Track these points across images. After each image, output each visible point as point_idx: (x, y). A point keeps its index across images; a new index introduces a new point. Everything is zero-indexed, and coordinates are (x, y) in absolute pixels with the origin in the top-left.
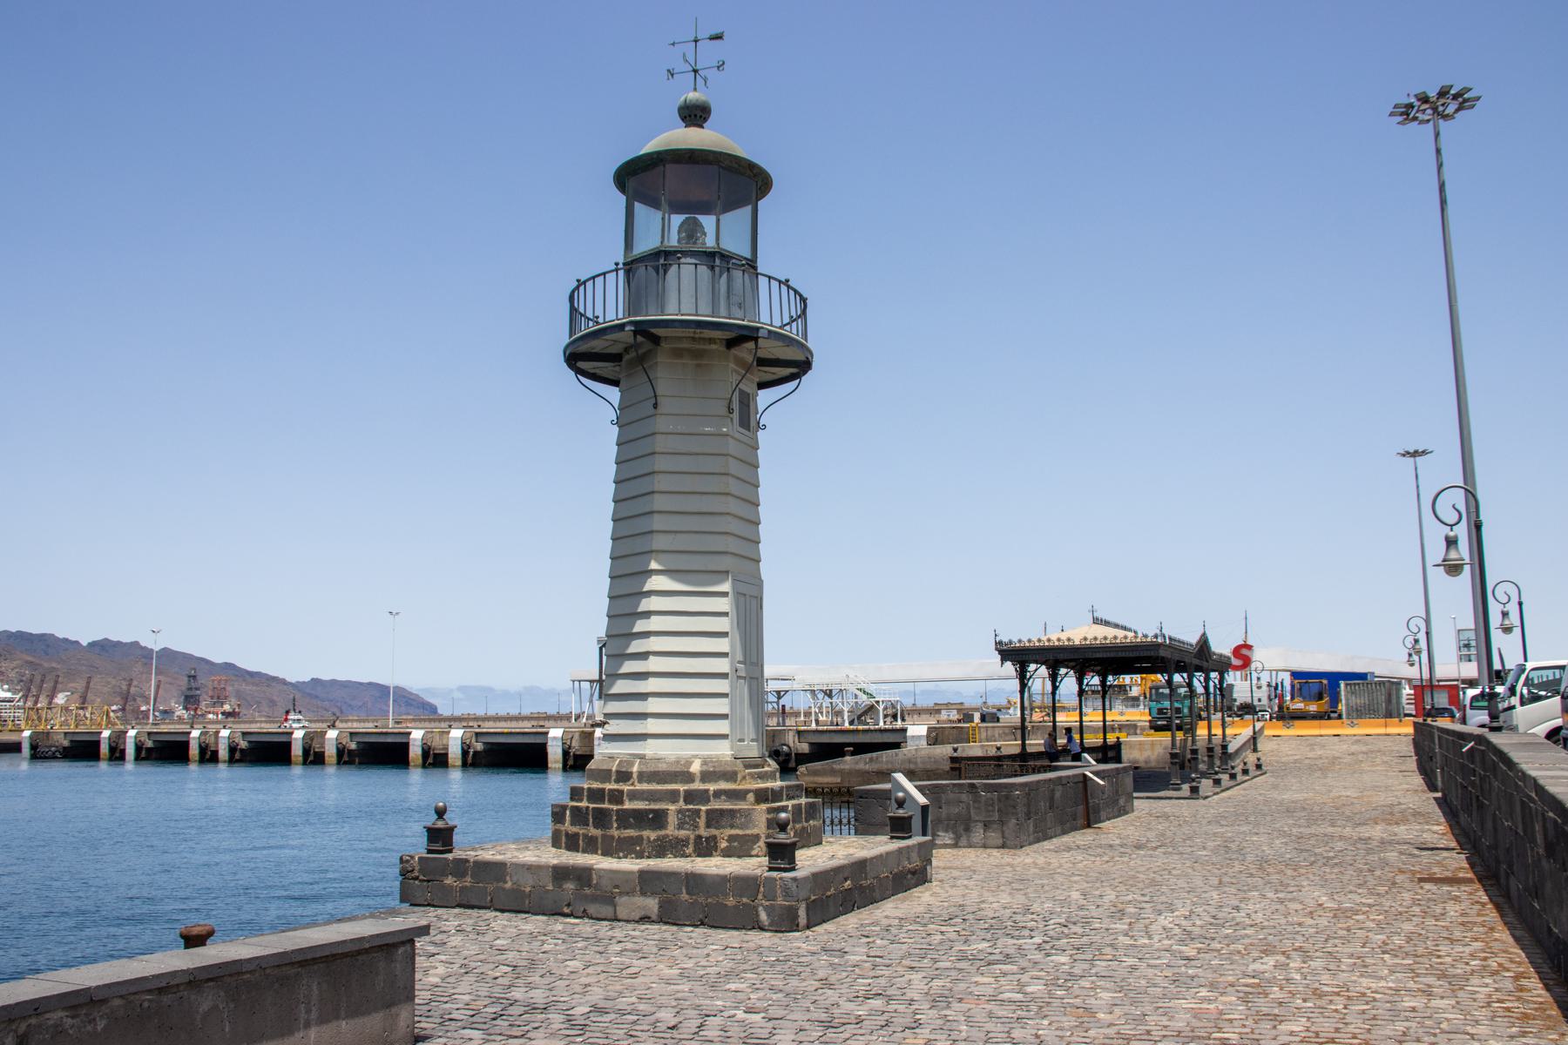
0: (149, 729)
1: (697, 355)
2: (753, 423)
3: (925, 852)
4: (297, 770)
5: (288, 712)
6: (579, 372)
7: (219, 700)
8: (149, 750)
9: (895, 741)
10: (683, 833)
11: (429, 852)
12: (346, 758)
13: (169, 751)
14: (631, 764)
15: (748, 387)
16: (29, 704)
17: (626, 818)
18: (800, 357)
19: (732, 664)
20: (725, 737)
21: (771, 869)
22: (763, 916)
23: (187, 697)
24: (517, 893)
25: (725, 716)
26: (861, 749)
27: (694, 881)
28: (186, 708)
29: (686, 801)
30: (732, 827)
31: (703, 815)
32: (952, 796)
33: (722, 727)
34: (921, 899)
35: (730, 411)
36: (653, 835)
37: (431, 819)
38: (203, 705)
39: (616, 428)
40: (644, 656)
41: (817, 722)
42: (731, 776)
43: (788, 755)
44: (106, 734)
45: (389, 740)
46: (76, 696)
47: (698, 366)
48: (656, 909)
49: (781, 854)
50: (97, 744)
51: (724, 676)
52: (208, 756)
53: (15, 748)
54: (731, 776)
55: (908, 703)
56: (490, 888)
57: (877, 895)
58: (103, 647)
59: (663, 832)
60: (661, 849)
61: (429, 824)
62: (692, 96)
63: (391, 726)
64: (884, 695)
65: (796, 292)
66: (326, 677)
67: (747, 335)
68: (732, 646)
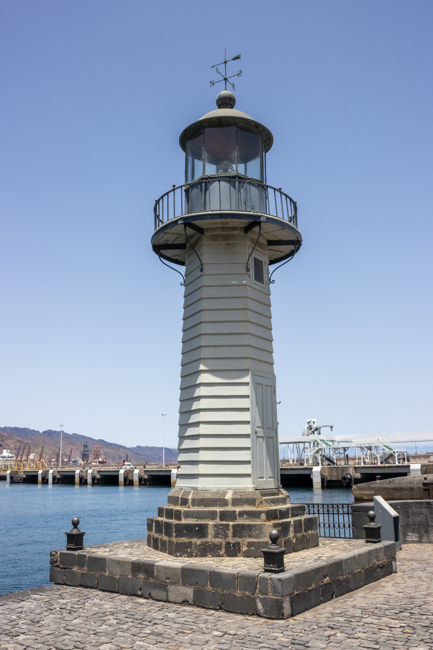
0: (59, 469)
1: (226, 238)
2: (265, 279)
3: (391, 553)
4: (121, 488)
5: (124, 461)
6: (161, 256)
7: (97, 456)
8: (58, 479)
9: (404, 472)
10: (218, 541)
11: (68, 549)
12: (143, 483)
13: (66, 480)
14: (188, 493)
15: (265, 259)
16: (19, 459)
17: (182, 530)
18: (294, 238)
19: (252, 428)
20: (248, 475)
21: (266, 571)
22: (260, 606)
23: (83, 455)
24: (111, 579)
25: (248, 462)
26: (384, 476)
27: (215, 577)
28: (83, 460)
29: (221, 519)
30: (250, 536)
31: (231, 528)
32: (415, 510)
33: (247, 469)
34: (386, 589)
35: (248, 270)
36: (198, 541)
37: (69, 529)
38: (90, 458)
39: (183, 288)
40: (197, 424)
41: (364, 463)
42: (251, 502)
43: (350, 479)
44: (40, 472)
45: (162, 474)
46: (38, 455)
47: (227, 244)
48: (192, 596)
49: (274, 561)
50: (37, 476)
51: (247, 436)
52: (83, 482)
53: (3, 478)
54: (251, 502)
55: (412, 452)
56: (97, 575)
57: (352, 585)
58: (49, 433)
59: (204, 540)
60: (205, 551)
61: (68, 531)
62: (224, 93)
63: (164, 468)
64: (397, 449)
65: (287, 196)
66: (143, 445)
67: (255, 222)
68: (252, 416)
